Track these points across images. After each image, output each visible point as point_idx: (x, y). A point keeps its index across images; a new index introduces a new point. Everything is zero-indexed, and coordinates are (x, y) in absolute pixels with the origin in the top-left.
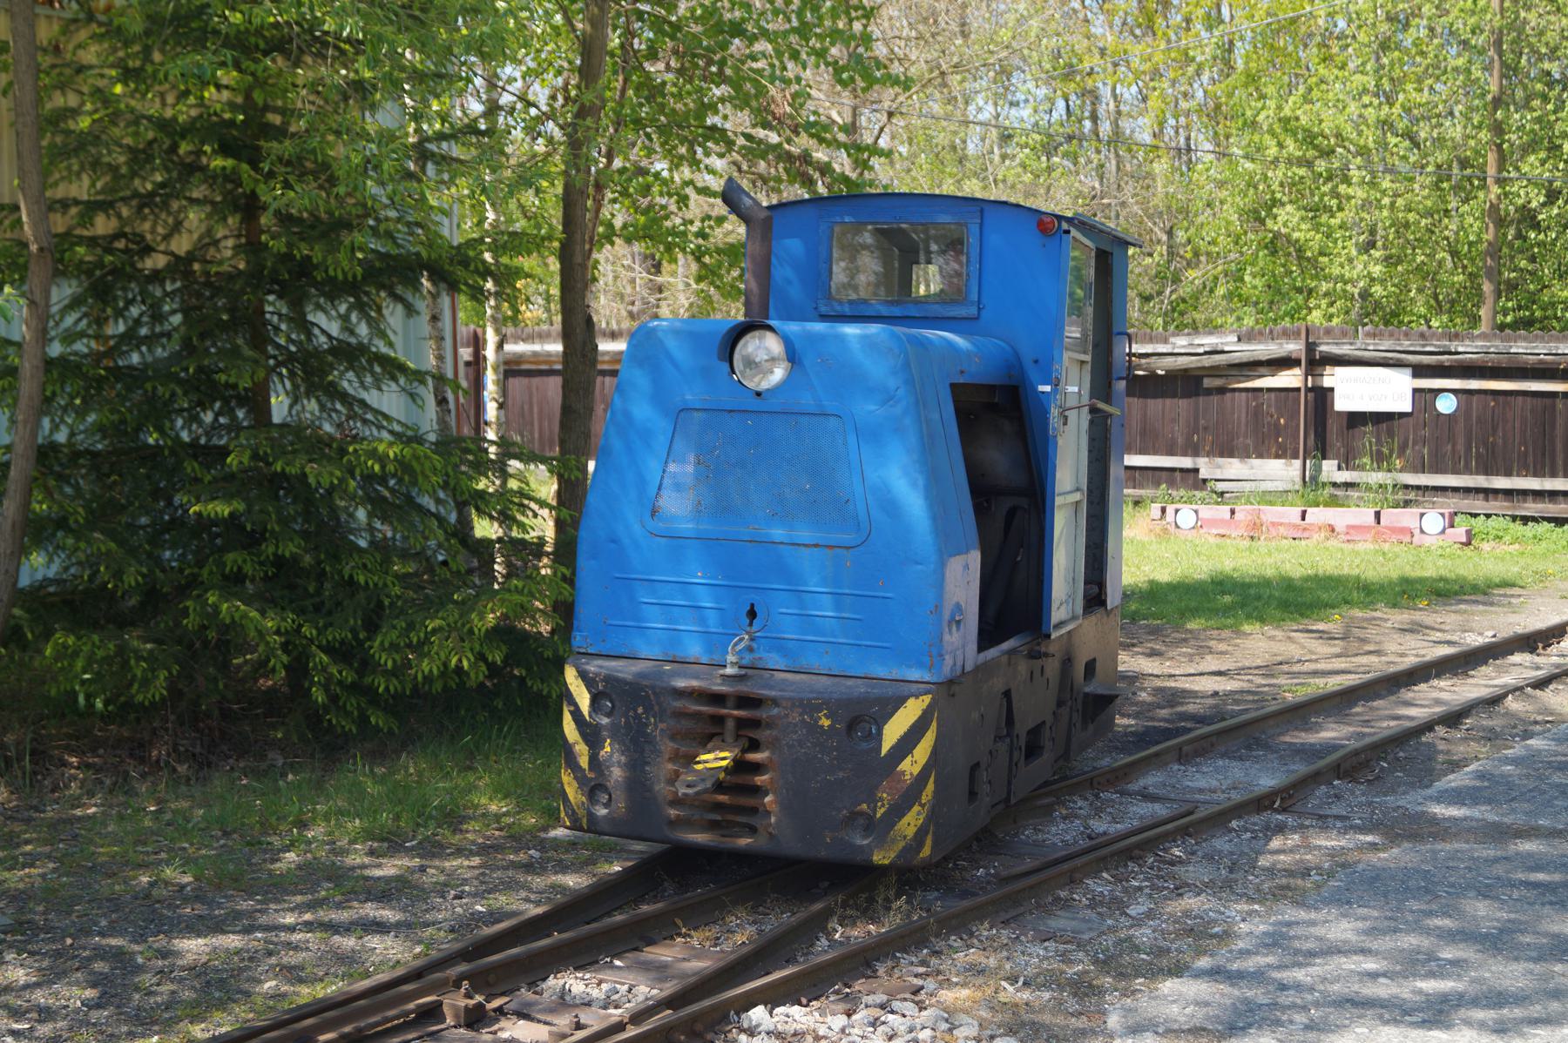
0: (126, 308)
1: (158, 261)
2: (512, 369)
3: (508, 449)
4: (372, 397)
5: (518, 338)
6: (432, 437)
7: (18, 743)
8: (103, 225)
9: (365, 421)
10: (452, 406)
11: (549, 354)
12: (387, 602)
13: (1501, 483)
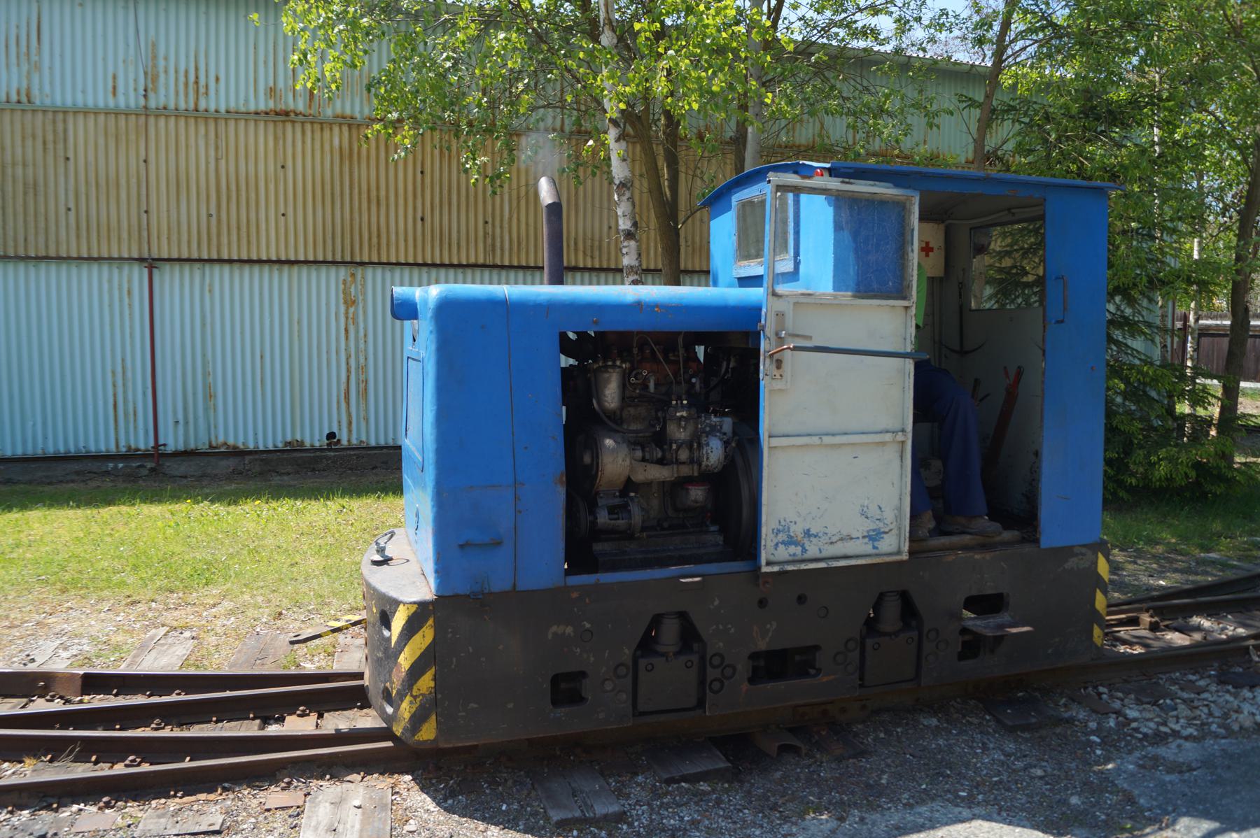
0: (1015, 299)
1: (1030, 278)
2: (1204, 333)
3: (1198, 372)
4: (1129, 342)
5: (1207, 317)
6: (1158, 363)
7: (874, 33)
8: (1007, 262)
9: (1126, 353)
10: (1169, 349)
11: (1225, 326)
12: (1136, 441)
13: (822, 565)
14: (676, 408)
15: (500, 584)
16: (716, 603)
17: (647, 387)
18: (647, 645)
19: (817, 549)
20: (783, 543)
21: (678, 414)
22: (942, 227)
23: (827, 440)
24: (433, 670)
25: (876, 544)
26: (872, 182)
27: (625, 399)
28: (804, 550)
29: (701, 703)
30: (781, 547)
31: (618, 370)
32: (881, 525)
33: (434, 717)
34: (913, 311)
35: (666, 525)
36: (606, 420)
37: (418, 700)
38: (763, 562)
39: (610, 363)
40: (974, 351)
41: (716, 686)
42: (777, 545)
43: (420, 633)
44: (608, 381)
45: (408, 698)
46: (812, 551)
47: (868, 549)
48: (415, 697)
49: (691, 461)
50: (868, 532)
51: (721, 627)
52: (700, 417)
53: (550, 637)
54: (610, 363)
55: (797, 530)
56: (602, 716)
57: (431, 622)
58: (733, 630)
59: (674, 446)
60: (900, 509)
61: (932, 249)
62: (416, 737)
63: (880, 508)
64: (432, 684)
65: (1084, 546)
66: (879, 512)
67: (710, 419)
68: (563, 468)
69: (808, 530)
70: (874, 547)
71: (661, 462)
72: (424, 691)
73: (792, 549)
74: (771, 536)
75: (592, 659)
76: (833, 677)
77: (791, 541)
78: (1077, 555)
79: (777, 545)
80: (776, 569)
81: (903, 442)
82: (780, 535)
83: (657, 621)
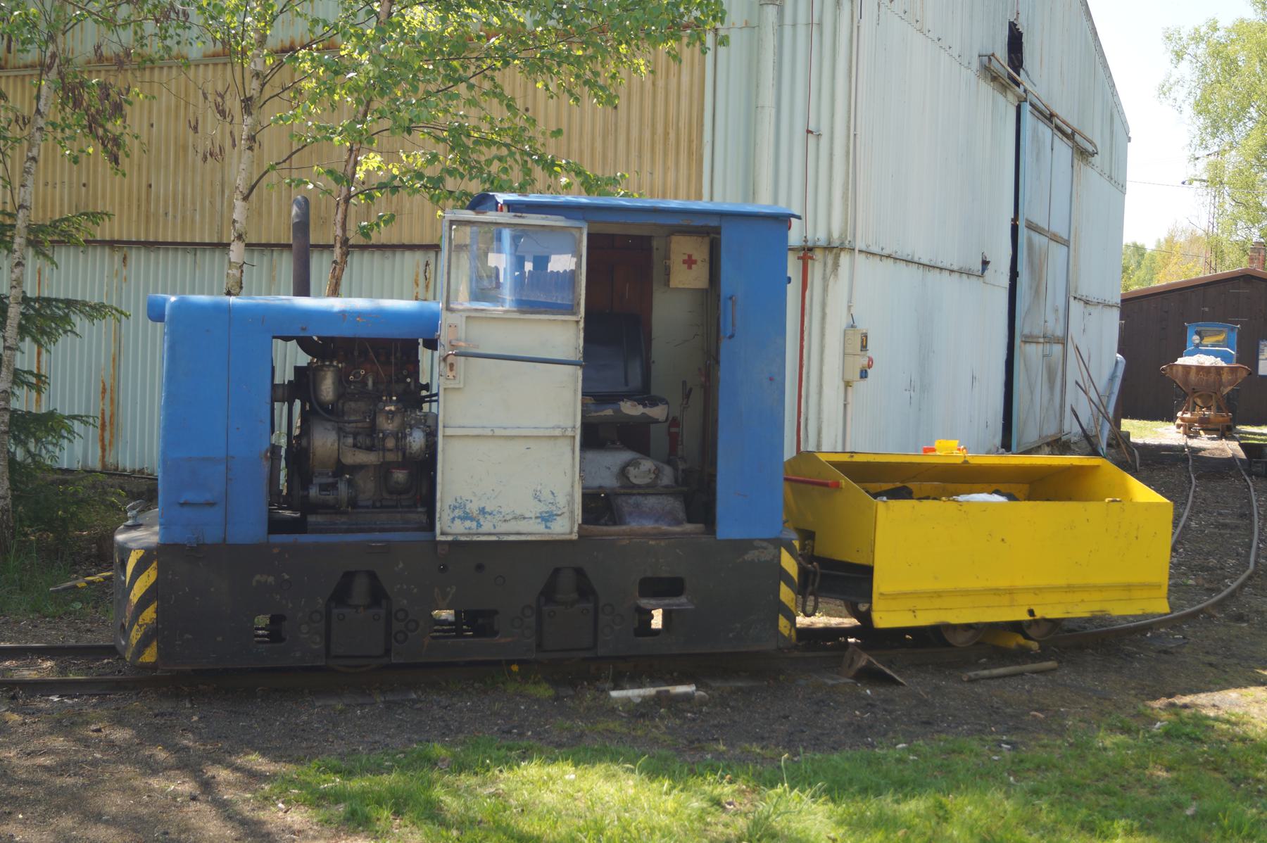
13: (494, 538)
14: (386, 403)
15: (212, 535)
16: (401, 565)
17: (366, 385)
18: (341, 595)
19: (491, 524)
20: (459, 517)
21: (387, 408)
22: (707, 240)
24: (156, 604)
25: (549, 524)
26: (544, 216)
27: (341, 395)
28: (479, 525)
29: (388, 652)
30: (458, 522)
31: (332, 369)
32: (554, 508)
33: (155, 643)
34: (582, 325)
35: (378, 504)
36: (321, 412)
37: (143, 628)
38: (438, 531)
39: (327, 363)
40: (116, 360)
42: (453, 519)
43: (146, 573)
44: (324, 378)
45: (136, 627)
46: (487, 526)
47: (540, 528)
48: (141, 626)
49: (397, 448)
50: (541, 513)
51: (405, 587)
52: (406, 411)
53: (254, 583)
54: (327, 363)
55: (473, 507)
56: (298, 654)
57: (154, 564)
58: (415, 590)
59: (381, 435)
60: (572, 496)
61: (695, 262)
62: (140, 660)
63: (553, 493)
64: (154, 616)
66: (551, 496)
67: (415, 412)
68: (836, 558)
69: (484, 508)
70: (546, 527)
71: (370, 449)
72: (147, 621)
73: (468, 523)
74: (447, 511)
75: (290, 605)
76: (509, 639)
77: (466, 517)
78: (756, 548)
79: (453, 519)
80: (450, 538)
81: (574, 437)
82: (457, 511)
83: (349, 576)
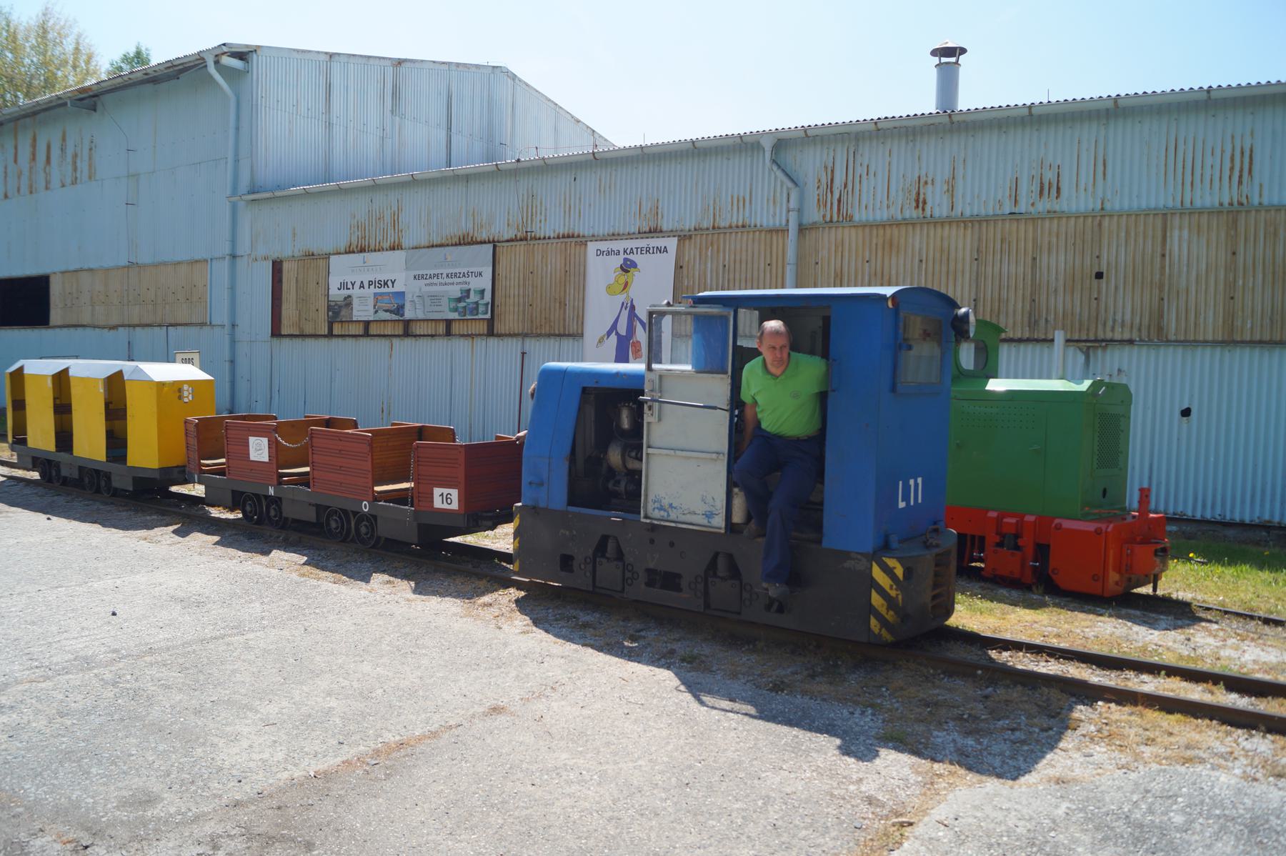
13: (673, 525)
16: (630, 535)
23: (679, 453)
28: (668, 515)
30: (656, 511)
41: (629, 581)
42: (654, 509)
46: (673, 517)
47: (705, 522)
55: (666, 502)
65: (857, 553)
70: (709, 522)
73: (662, 513)
77: (661, 508)
79: (654, 509)
80: (648, 521)
